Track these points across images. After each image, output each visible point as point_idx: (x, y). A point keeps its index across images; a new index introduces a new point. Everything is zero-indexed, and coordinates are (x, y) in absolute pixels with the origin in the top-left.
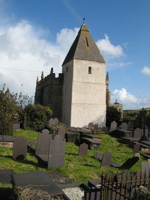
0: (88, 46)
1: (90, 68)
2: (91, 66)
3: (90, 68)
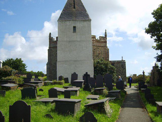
0: (74, 8)
1: (74, 28)
2: (75, 26)
3: (74, 28)
